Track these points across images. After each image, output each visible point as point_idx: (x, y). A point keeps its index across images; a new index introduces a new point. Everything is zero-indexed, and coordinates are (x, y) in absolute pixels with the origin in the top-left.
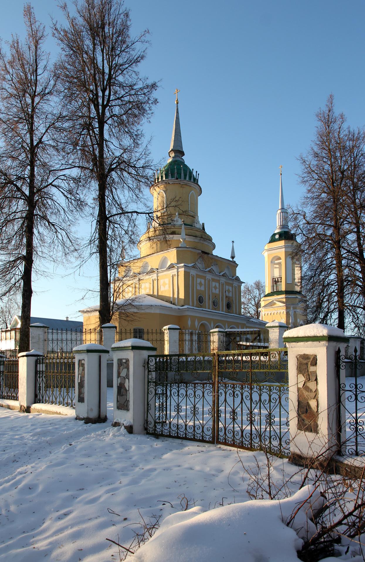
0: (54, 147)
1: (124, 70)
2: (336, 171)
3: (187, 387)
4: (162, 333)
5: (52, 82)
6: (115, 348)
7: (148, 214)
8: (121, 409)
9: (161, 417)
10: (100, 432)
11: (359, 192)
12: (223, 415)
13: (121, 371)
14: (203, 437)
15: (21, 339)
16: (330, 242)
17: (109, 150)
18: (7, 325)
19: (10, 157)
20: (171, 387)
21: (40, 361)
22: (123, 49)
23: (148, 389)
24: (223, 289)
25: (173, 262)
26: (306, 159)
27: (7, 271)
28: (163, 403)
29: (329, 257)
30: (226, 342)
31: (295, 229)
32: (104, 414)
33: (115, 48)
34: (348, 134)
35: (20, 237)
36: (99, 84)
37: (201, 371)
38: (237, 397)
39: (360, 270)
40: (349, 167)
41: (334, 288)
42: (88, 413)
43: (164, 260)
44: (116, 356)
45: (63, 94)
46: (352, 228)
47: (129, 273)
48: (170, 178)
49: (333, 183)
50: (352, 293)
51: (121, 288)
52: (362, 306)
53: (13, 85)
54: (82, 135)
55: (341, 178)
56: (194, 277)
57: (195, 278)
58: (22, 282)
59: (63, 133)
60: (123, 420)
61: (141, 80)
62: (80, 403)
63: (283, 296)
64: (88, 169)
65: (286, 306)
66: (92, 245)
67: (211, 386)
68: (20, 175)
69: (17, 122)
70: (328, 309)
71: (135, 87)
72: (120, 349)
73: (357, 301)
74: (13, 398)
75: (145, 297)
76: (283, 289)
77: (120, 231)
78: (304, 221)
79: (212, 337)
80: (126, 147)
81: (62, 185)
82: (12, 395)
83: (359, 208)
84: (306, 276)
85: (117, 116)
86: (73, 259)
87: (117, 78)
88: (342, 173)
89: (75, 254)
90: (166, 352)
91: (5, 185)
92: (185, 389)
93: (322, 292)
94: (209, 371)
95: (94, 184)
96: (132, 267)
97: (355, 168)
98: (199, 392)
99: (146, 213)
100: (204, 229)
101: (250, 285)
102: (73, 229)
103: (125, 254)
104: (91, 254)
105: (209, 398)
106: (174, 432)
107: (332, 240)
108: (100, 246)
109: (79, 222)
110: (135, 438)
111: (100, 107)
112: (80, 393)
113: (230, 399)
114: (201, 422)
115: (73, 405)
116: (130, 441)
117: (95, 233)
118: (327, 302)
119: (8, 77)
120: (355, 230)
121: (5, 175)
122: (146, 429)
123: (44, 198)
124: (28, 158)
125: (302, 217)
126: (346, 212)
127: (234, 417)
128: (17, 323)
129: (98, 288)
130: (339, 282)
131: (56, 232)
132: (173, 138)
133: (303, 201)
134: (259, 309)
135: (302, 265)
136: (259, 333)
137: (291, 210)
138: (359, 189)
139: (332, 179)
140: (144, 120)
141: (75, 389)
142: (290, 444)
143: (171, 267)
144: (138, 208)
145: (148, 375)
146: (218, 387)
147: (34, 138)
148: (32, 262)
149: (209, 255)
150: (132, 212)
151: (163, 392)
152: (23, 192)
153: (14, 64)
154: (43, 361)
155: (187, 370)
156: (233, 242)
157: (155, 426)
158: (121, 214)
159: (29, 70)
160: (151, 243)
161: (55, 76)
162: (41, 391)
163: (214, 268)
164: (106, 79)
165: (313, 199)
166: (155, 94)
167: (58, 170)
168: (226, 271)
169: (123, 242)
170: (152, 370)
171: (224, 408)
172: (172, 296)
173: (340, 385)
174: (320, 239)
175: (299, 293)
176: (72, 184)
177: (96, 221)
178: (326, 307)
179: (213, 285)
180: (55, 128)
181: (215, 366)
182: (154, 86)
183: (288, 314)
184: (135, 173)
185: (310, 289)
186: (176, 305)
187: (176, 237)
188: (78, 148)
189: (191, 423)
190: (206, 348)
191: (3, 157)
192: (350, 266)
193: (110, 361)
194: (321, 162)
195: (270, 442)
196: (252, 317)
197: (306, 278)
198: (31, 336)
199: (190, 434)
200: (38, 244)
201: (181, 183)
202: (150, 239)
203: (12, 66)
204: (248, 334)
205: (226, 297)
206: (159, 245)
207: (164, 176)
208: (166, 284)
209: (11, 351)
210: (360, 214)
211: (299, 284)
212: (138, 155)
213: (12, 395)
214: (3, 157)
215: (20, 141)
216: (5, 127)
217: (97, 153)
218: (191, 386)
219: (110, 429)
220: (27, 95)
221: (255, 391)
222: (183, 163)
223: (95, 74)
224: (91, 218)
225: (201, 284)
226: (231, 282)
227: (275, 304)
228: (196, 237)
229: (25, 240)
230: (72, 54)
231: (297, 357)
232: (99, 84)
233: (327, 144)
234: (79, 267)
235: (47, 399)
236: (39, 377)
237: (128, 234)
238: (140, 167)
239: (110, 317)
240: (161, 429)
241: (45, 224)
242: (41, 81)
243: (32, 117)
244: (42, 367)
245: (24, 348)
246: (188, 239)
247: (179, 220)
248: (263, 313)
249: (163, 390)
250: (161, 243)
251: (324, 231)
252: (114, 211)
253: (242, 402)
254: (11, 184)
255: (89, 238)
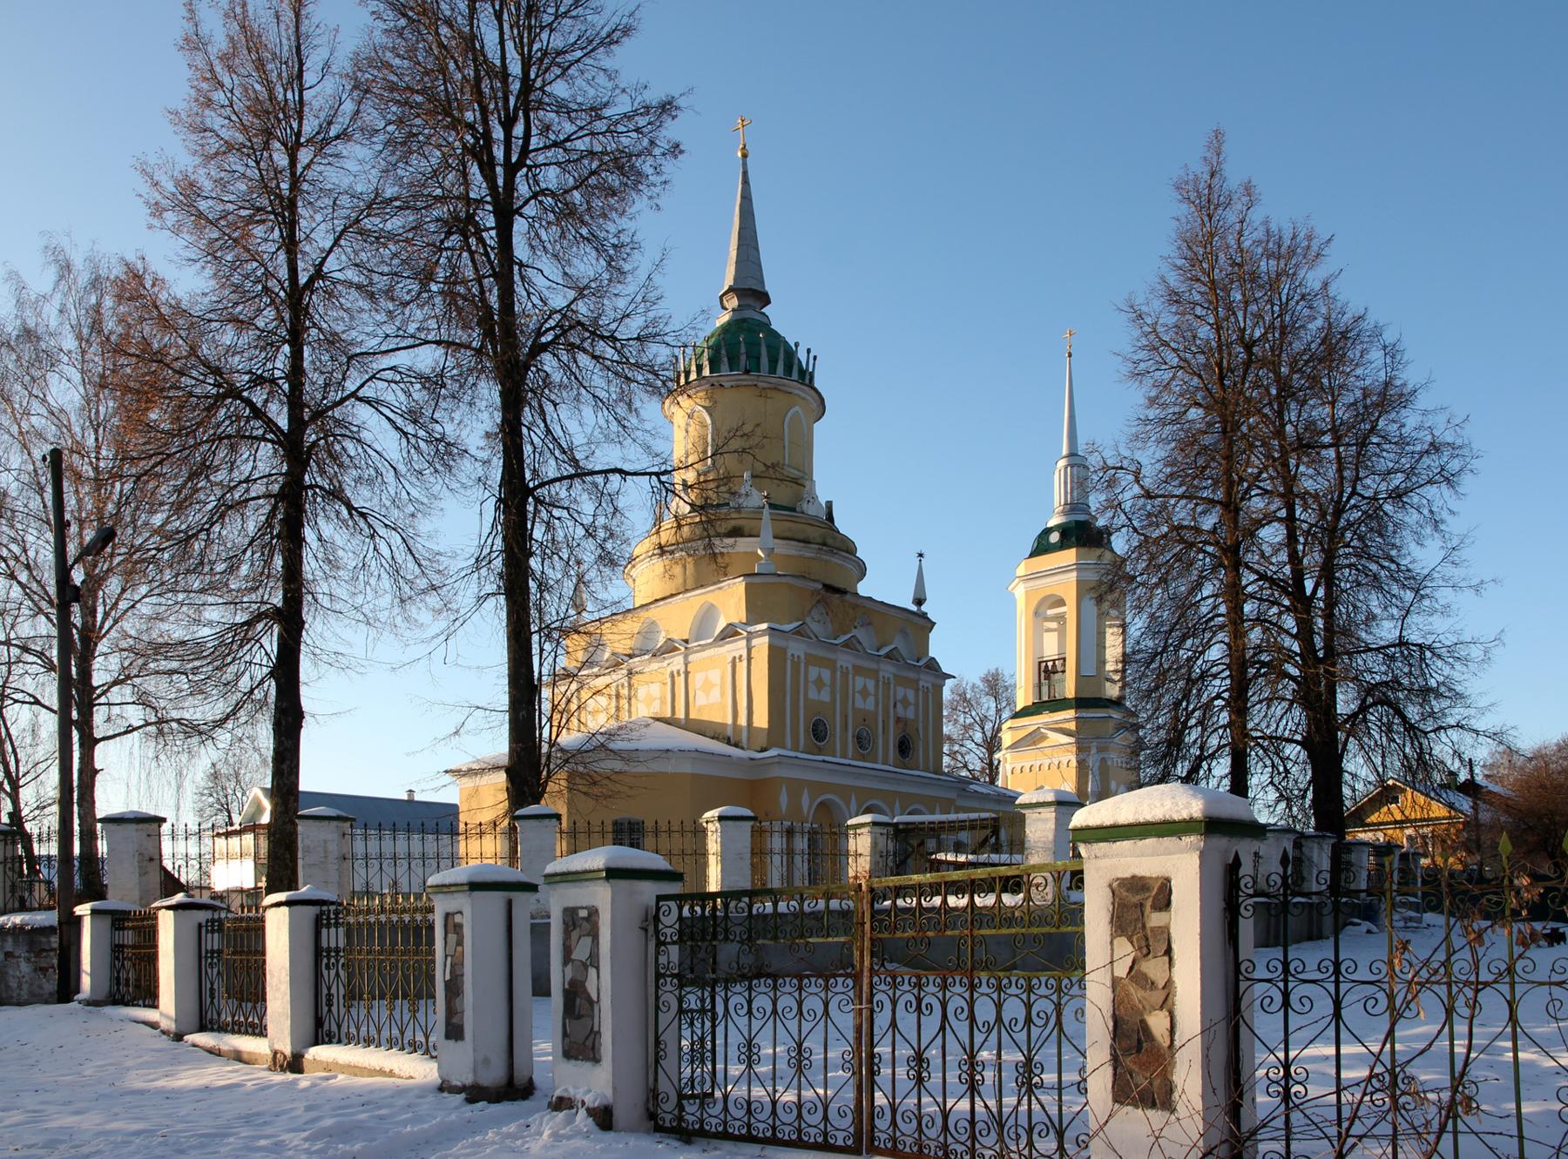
0: (359, 287)
1: (569, 67)
2: (1232, 343)
3: (775, 988)
4: (700, 833)
5: (348, 107)
6: (556, 875)
7: (657, 474)
8: (576, 1059)
9: (698, 1079)
10: (512, 1128)
11: (1293, 405)
12: (886, 1071)
13: (573, 943)
14: (825, 1134)
15: (272, 855)
16: (1210, 549)
17: (531, 290)
18: (230, 817)
19: (230, 321)
20: (726, 989)
21: (329, 918)
22: (562, 9)
23: (657, 998)
24: (887, 697)
25: (735, 620)
26: (1144, 309)
27: (228, 655)
28: (702, 1039)
29: (1206, 593)
30: (895, 854)
31: (1109, 514)
32: (526, 1074)
33: (538, 9)
34: (1265, 238)
35: (263, 554)
36: (492, 106)
37: (821, 940)
38: (927, 1013)
39: (1295, 631)
40: (1266, 333)
41: (1219, 684)
42: (475, 1071)
43: (707, 615)
44: (556, 901)
45: (381, 137)
46: (1273, 507)
47: (598, 652)
48: (725, 367)
49: (1222, 378)
50: (1269, 701)
51: (575, 700)
52: (1298, 737)
53: (234, 118)
54: (447, 249)
55: (1243, 363)
56: (799, 663)
57: (802, 665)
58: (272, 686)
59: (385, 245)
60: (581, 1090)
61: (624, 91)
62: (451, 1043)
63: (1071, 713)
64: (468, 347)
65: (1077, 742)
66: (484, 572)
67: (850, 982)
68: (259, 372)
69: (250, 220)
70: (1202, 748)
71: (607, 112)
72: (570, 878)
73: (1284, 721)
74: (250, 1030)
75: (647, 726)
76: (1070, 693)
77: (571, 529)
78: (1137, 490)
79: (851, 841)
80: (586, 281)
81: (389, 397)
82: (247, 1019)
83: (1293, 450)
84: (1140, 651)
85: (553, 194)
86: (425, 616)
87: (547, 89)
88: (1248, 347)
89: (433, 600)
90: (713, 886)
91: (216, 401)
92: (771, 994)
93: (1183, 698)
94: (842, 939)
95: (486, 392)
96: (609, 636)
97: (1283, 333)
98: (813, 1003)
99: (650, 474)
100: (830, 517)
101: (970, 685)
102: (424, 525)
103: (585, 596)
104: (481, 599)
105: (845, 1020)
106: (738, 1124)
107: (1217, 544)
108: (509, 574)
109: (442, 504)
110: (618, 1142)
111: (499, 170)
112: (452, 1012)
113: (907, 1021)
114: (821, 1091)
115: (431, 1049)
116: (603, 1150)
117: (491, 537)
118: (1200, 728)
119: (219, 97)
120: (1283, 513)
121: (217, 371)
122: (652, 1116)
123: (334, 436)
124: (283, 320)
125: (1131, 478)
126: (1257, 462)
127: (919, 1074)
128: (259, 809)
129: (503, 700)
130: (1235, 667)
131: (372, 537)
132: (734, 254)
133: (1134, 430)
134: (996, 756)
135: (1128, 620)
136: (994, 826)
137: (1099, 458)
138: (1294, 394)
139: (1220, 365)
140: (639, 204)
141: (434, 1004)
142: (1091, 1145)
143: (730, 633)
144: (624, 460)
145: (657, 953)
146: (871, 986)
147: (301, 265)
148: (303, 627)
149: (848, 597)
150: (606, 472)
151: (703, 1006)
152: (270, 420)
153: (237, 61)
154: (337, 918)
155: (775, 938)
156: (921, 555)
157: (681, 1108)
158: (571, 477)
159: (280, 76)
160: (667, 562)
161: (355, 87)
162: (334, 1009)
163: (860, 633)
164: (515, 92)
165: (1164, 425)
166: (671, 131)
167: (374, 354)
168: (898, 643)
169: (579, 563)
170: (669, 940)
171: (890, 1050)
172: (729, 721)
173: (1237, 965)
174: (1182, 540)
175: (1117, 703)
176: (419, 394)
177: (494, 499)
178: (1195, 742)
179: (859, 686)
180: (361, 234)
181: (863, 924)
182: (667, 108)
183: (1082, 766)
184: (616, 357)
185: (1150, 691)
186: (743, 748)
187: (743, 544)
188: (434, 287)
189: (789, 1097)
190: (834, 873)
191: (210, 321)
192: (1266, 621)
193: (542, 917)
194: (1187, 317)
195: (1030, 1144)
196: (974, 778)
197: (1138, 657)
198: (300, 845)
199: (787, 1129)
200: (319, 573)
201: (761, 385)
202: (662, 550)
203: (229, 67)
204: (962, 828)
205: (898, 720)
206: (690, 567)
207: (706, 364)
208: (713, 685)
209: (242, 891)
210: (1297, 466)
211: (1117, 677)
212: (621, 303)
213: (247, 1019)
214: (210, 321)
215: (259, 273)
216: (215, 235)
217: (493, 299)
218: (788, 985)
219: (543, 1117)
220: (277, 145)
221: (983, 994)
222: (765, 325)
223: (478, 79)
224: (478, 493)
225: (819, 683)
226: (912, 675)
227: (1044, 738)
228: (806, 541)
229: (278, 562)
230: (403, 28)
231: (1110, 886)
232: (492, 106)
233: (1205, 266)
234: (443, 637)
235: (353, 1030)
236: (328, 967)
237: (594, 537)
238: (628, 340)
239: (539, 785)
240: (698, 1114)
241: (338, 513)
242: (316, 105)
243: (292, 206)
244: (334, 938)
245: (281, 881)
246: (782, 548)
247: (755, 492)
248: (1009, 768)
249: (703, 1000)
250: (696, 564)
251: (1194, 519)
252: (551, 470)
253: (943, 1028)
254: (235, 398)
255: (473, 550)
